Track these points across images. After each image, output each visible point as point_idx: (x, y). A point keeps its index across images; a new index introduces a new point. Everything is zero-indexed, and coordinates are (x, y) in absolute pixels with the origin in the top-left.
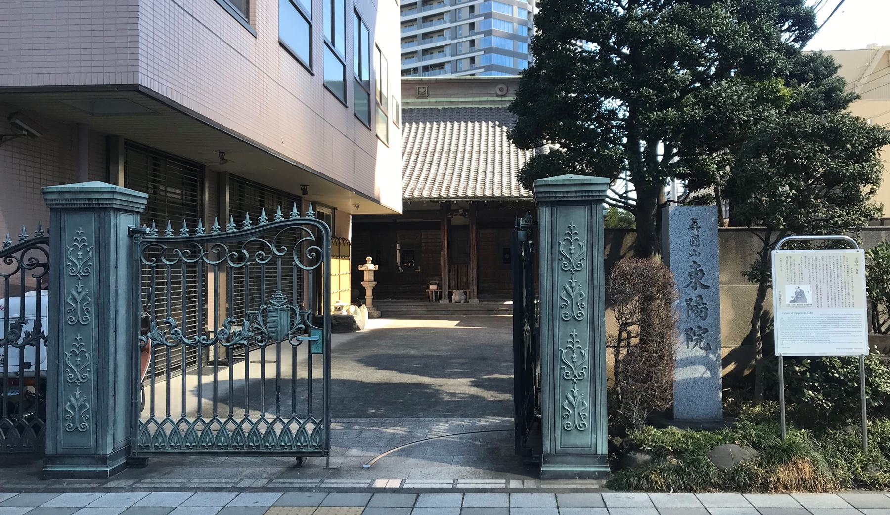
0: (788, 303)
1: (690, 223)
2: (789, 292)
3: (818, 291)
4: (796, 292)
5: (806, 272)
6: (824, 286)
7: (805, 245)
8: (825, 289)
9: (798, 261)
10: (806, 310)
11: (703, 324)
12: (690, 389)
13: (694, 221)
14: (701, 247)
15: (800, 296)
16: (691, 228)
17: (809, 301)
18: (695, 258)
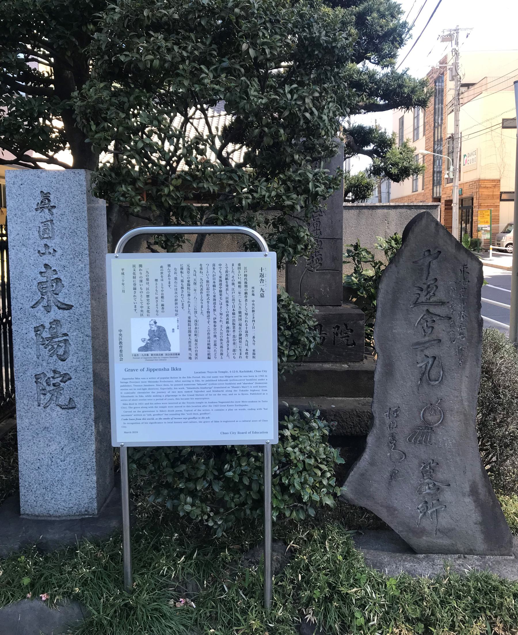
0: (135, 351)
1: (39, 199)
2: (138, 331)
3: (191, 330)
4: (151, 332)
5: (169, 294)
6: (202, 319)
7: (170, 244)
8: (203, 325)
9: (155, 274)
10: (168, 364)
11: (62, 367)
12: (43, 469)
13: (46, 196)
14: (57, 240)
15: (158, 338)
16: (41, 207)
17: (175, 348)
18: (47, 259)
